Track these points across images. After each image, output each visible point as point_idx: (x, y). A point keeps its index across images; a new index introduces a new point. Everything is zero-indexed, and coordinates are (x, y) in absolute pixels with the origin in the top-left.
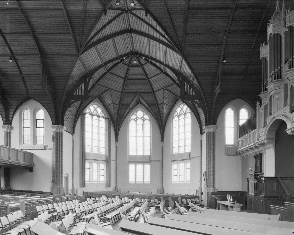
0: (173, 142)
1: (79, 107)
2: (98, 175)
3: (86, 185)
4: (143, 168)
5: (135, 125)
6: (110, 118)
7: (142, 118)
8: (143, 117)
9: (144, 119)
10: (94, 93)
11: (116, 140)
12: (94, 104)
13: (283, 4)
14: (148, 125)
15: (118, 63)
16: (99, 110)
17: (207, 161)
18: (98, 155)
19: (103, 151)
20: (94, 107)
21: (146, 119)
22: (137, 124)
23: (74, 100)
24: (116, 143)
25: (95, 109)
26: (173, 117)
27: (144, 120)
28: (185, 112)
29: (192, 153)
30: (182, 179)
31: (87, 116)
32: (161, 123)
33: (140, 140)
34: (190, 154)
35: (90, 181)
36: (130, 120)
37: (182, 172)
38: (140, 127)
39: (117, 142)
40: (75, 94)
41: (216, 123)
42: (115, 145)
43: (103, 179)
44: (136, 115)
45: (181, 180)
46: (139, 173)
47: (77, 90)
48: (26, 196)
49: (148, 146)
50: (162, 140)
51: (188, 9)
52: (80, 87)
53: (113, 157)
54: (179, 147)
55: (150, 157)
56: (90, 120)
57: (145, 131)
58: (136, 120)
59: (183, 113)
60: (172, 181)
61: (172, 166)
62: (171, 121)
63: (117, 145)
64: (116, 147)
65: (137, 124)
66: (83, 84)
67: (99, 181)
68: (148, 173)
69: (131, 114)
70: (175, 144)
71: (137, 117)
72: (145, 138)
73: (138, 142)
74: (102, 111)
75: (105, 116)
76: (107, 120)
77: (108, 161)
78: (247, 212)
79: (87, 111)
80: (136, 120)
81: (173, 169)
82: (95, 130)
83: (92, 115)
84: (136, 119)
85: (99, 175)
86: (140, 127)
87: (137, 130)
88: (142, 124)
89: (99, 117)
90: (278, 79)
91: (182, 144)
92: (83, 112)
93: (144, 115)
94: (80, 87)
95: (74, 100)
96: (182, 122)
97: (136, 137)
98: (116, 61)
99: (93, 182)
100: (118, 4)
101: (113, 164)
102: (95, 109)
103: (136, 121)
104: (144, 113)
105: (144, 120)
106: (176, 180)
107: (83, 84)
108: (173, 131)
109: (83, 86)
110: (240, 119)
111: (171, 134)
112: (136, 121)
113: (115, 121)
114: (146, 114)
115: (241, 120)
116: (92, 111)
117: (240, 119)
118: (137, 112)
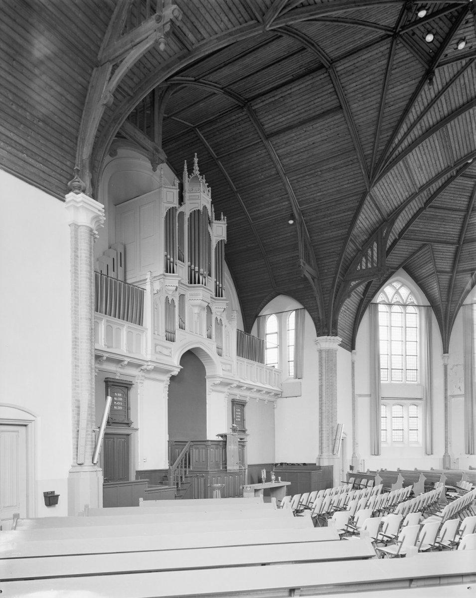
1: (364, 294)
3: (382, 451)
6: (429, 304)
10: (393, 259)
11: (446, 350)
12: (393, 282)
13: (196, 160)
15: (452, 178)
16: (404, 292)
23: (357, 282)
25: (397, 292)
31: (381, 308)
39: (446, 355)
40: (359, 267)
41: (324, 334)
43: (417, 438)
47: (364, 259)
51: (340, 106)
52: (369, 252)
66: (375, 244)
74: (412, 293)
75: (418, 302)
76: (423, 310)
78: (178, 497)
79: (379, 298)
90: (195, 283)
92: (372, 302)
94: (369, 252)
95: (357, 282)
98: (439, 181)
100: (462, 46)
102: (397, 292)
107: (375, 244)
109: (375, 249)
110: (266, 334)
113: (443, 311)
115: (267, 336)
116: (404, 298)
117: (266, 334)
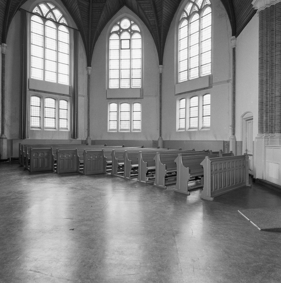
0: (179, 63)
2: (57, 118)
4: (130, 109)
5: (118, 42)
7: (130, 31)
8: (130, 28)
9: (131, 30)
11: (89, 64)
14: (137, 41)
17: (261, 75)
18: (57, 85)
19: (65, 80)
20: (49, 7)
21: (135, 32)
22: (121, 40)
24: (87, 69)
26: (179, 22)
27: (132, 33)
28: (201, 7)
29: (232, 35)
30: (194, 123)
32: (160, 36)
33: (125, 64)
34: (210, 78)
35: (55, 128)
36: (110, 34)
37: (194, 112)
38: (125, 44)
39: (89, 67)
42: (86, 73)
44: (119, 25)
45: (192, 126)
46: (125, 116)
48: (122, 146)
49: (137, 74)
50: (161, 63)
53: (82, 91)
54: (189, 70)
55: (141, 90)
56: (41, 27)
57: (133, 51)
58: (119, 33)
59: (196, 9)
60: (177, 127)
61: (178, 102)
62: (175, 29)
63: (90, 73)
64: (89, 76)
65: (121, 40)
67: (57, 127)
68: (137, 116)
69: (111, 25)
70: (182, 66)
71: (120, 28)
72: (134, 61)
73: (122, 67)
76: (72, 31)
77: (73, 97)
80: (119, 33)
81: (178, 108)
82: (51, 44)
83: (44, 19)
84: (119, 31)
85: (42, 117)
86: (125, 44)
87: (121, 49)
88: (129, 39)
89: (58, 24)
91: (194, 62)
93: (131, 25)
96: (195, 27)
97: (120, 59)
99: (45, 130)
101: (82, 101)
102: (51, 11)
103: (119, 35)
104: (132, 22)
105: (132, 33)
106: (182, 126)
108: (179, 45)
111: (175, 51)
112: (119, 35)
114: (135, 23)
118: (120, 20)
